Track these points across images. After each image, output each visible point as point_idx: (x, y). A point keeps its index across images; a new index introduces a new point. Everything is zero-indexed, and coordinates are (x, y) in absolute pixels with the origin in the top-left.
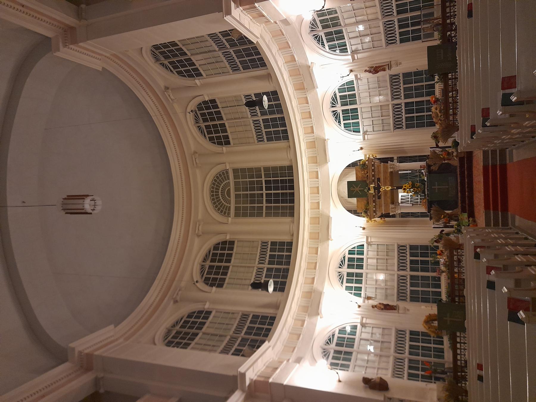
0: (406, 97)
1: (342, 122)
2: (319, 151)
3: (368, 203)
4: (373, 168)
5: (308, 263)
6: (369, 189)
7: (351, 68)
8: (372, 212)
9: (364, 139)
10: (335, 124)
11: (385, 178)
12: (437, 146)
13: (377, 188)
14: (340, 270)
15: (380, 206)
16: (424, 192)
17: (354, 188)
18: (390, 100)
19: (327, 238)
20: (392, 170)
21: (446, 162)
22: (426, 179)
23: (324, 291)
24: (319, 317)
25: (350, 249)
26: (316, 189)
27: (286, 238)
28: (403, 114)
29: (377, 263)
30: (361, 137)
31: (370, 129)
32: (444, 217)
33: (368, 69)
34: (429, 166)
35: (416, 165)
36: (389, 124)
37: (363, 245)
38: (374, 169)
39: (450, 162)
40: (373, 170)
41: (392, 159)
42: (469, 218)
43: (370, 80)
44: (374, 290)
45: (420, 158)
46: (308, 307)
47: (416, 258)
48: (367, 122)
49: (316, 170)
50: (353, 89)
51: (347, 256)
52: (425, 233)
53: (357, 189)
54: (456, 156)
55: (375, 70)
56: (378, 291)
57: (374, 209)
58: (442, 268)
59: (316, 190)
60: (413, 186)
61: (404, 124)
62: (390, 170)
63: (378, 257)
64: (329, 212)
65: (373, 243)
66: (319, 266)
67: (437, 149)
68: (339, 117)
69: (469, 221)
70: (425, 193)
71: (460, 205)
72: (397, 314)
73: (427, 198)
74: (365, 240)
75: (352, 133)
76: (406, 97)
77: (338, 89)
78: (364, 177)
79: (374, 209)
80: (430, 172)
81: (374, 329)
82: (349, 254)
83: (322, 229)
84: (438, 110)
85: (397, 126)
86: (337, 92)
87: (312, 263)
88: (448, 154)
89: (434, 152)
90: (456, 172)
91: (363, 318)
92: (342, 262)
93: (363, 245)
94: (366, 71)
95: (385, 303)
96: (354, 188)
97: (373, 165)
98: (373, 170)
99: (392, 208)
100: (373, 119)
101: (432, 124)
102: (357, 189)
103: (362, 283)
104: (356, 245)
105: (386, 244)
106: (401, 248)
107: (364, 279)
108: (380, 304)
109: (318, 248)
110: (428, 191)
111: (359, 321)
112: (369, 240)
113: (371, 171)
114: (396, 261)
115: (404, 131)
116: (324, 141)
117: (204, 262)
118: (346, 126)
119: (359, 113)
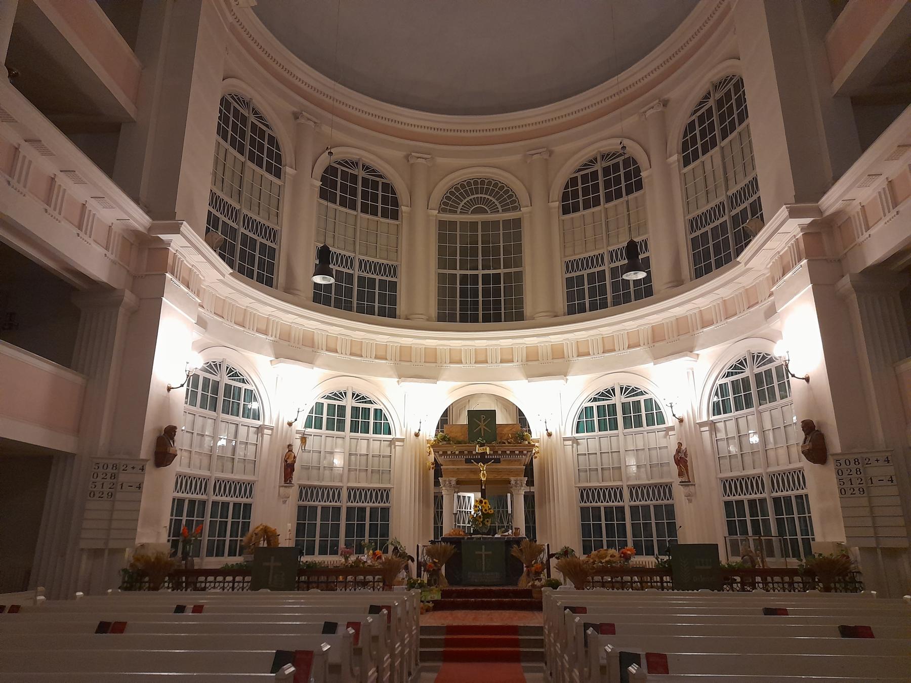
0: (634, 509)
1: (595, 405)
3: (459, 443)
4: (517, 452)
9: (565, 439)
10: (592, 392)
11: (498, 471)
12: (550, 556)
13: (483, 458)
14: (349, 395)
15: (453, 463)
16: (476, 532)
20: (513, 482)
22: (496, 536)
27: (402, 307)
28: (605, 504)
30: (568, 434)
31: (582, 449)
32: (435, 563)
33: (683, 448)
34: (518, 541)
35: (520, 521)
37: (390, 433)
39: (524, 574)
40: (512, 452)
41: (530, 483)
42: (433, 601)
43: (664, 451)
47: (365, 516)
48: (593, 445)
49: (515, 359)
50: (650, 422)
51: (372, 407)
52: (409, 531)
53: (482, 425)
54: (533, 586)
55: (681, 459)
57: (449, 452)
61: (588, 504)
62: (512, 479)
63: (370, 456)
64: (444, 380)
65: (393, 450)
69: (428, 602)
72: (278, 484)
74: (398, 436)
75: (576, 420)
76: (634, 509)
79: (449, 452)
80: (509, 543)
82: (376, 410)
83: (421, 368)
85: (585, 493)
88: (538, 573)
89: (541, 551)
93: (390, 433)
94: (680, 444)
97: (521, 453)
98: (512, 452)
100: (598, 454)
102: (482, 425)
103: (327, 429)
104: (390, 421)
106: (384, 494)
108: (295, 457)
111: (267, 423)
112: (397, 443)
118: (588, 411)
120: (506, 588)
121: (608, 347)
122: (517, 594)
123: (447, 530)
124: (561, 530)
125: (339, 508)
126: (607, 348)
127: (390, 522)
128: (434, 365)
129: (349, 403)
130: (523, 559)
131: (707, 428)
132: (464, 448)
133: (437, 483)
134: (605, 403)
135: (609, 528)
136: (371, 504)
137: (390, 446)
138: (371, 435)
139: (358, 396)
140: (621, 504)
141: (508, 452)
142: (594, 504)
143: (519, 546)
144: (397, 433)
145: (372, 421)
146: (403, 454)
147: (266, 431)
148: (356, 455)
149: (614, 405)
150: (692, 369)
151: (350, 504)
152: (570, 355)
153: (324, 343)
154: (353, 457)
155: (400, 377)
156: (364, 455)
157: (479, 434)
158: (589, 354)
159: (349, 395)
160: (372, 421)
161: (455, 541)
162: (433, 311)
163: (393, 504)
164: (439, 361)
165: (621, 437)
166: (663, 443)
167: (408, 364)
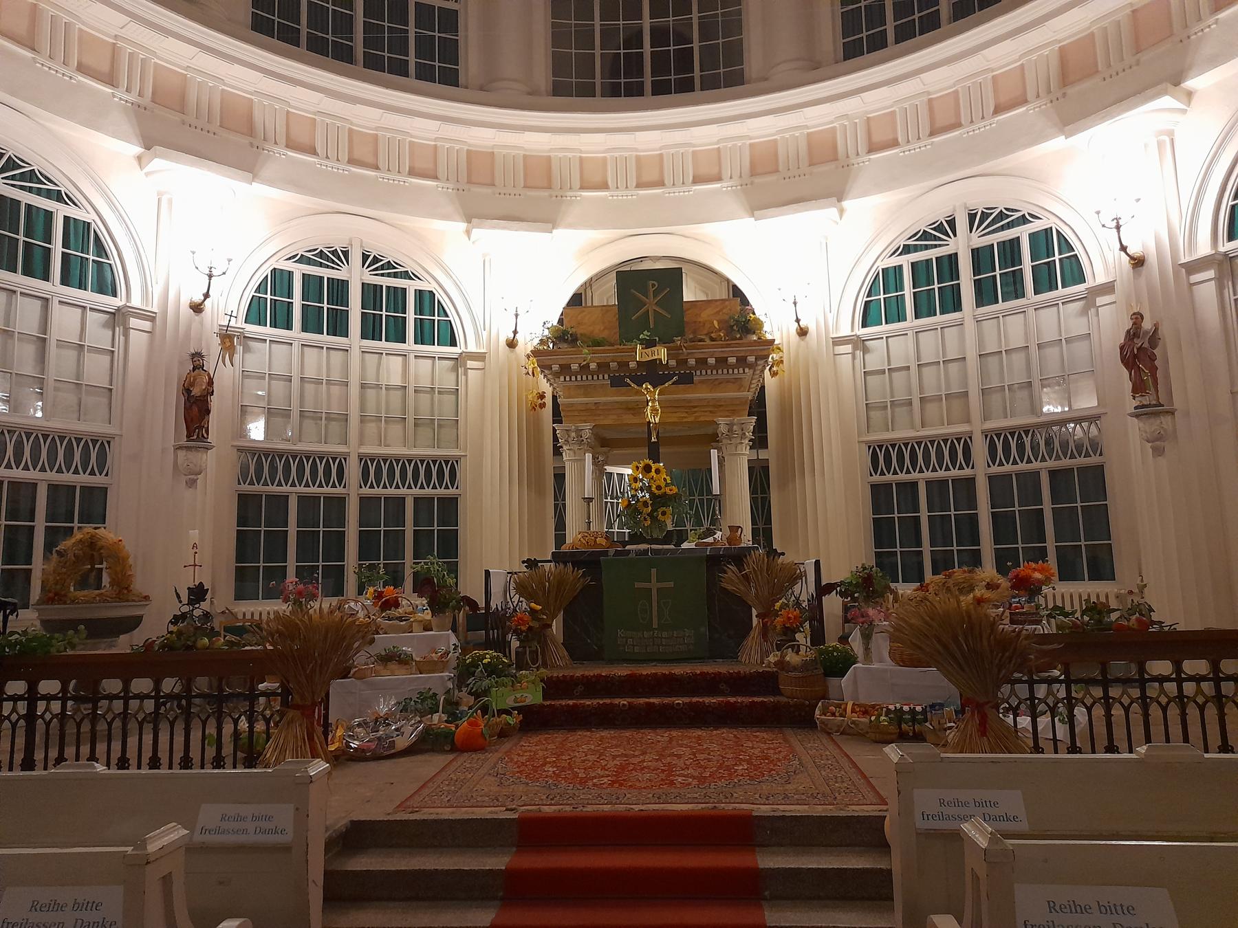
1: (906, 261)
2: (800, 178)
3: (597, 343)
4: (732, 360)
5: (376, 137)
6: (649, 344)
7: (1152, 259)
8: (563, 359)
9: (837, 342)
10: (899, 233)
11: (689, 406)
12: (823, 590)
13: (653, 373)
14: (356, 258)
15: (586, 390)
16: (635, 538)
17: (655, 294)
18: (990, 425)
19: (473, 215)
20: (723, 429)
21: (755, 621)
22: (685, 545)
23: (256, 186)
24: (138, 150)
26: (654, 176)
27: (471, 62)
29: (388, 388)
30: (845, 331)
31: (875, 360)
32: (533, 611)
33: (1147, 325)
34: (738, 557)
35: (739, 510)
36: (891, 425)
37: (453, 343)
38: (729, 366)
39: (755, 633)
40: (722, 361)
41: (760, 440)
42: (520, 710)
43: (1081, 348)
44: (955, 389)
45: (763, 529)
46: (182, 110)
47: (415, 517)
48: (902, 351)
49: (726, 173)
50: (1045, 280)
51: (411, 286)
52: (496, 547)
53: (651, 305)
54: (781, 664)
55: (1140, 353)
56: (278, 386)
57: (575, 367)
58: (772, 658)
59: (650, 174)
60: (659, 500)
61: (889, 477)
62: (722, 423)
63: (411, 391)
65: (462, 378)
66: (363, 177)
67: (812, 588)
68: (927, 247)
69: (508, 712)
70: (631, 542)
71: (578, 673)
72: (171, 442)
73: (612, 551)
74: (472, 348)
77: (1048, 232)
78: (694, 332)
79: (575, 367)
80: (715, 561)
81: (107, 358)
82: (420, 294)
83: (516, 196)
84: (988, 594)
85: (882, 455)
86: (1036, 226)
87: (376, 154)
88: (789, 633)
89: (794, 576)
90: (713, 656)
91: (151, 318)
92: (389, 265)
93: (453, 343)
94: (1138, 318)
95: (215, 402)
96: (655, 294)
97: (742, 361)
98: (722, 361)
99: (578, 431)
100: (914, 368)
101: (245, 585)
102: (651, 305)
103: (305, 329)
104: (453, 317)
105: (461, 418)
106: (447, 470)
107: (325, 338)
108: (211, 382)
109: (435, 178)
110: (639, 553)
111: (136, 301)
112: (470, 364)
113: (719, 352)
114: (397, 450)
115: (862, 479)
116: (836, 194)
117: (365, 257)
118: (891, 277)
119: (939, 318)
121: (942, 119)
122: (740, 684)
123: (573, 533)
125: (971, 481)
126: (940, 123)
127: (460, 528)
128: (545, 193)
129: (356, 275)
131: (1211, 274)
132: (605, 355)
133: (557, 451)
134: (932, 254)
135: (939, 524)
136: (416, 491)
137: (455, 369)
138: (410, 345)
139: (376, 260)
140: (967, 472)
141: (712, 361)
143: (741, 569)
144: (469, 342)
145: (411, 316)
146: (484, 387)
147: (134, 322)
148: (378, 387)
149: (953, 258)
150: (1171, 134)
151: (366, 491)
152: (851, 152)
153: (281, 130)
154: (371, 393)
155: (468, 219)
157: (644, 324)
158: (894, 143)
159: (356, 258)
160: (411, 316)
161: (587, 561)
162: (542, 75)
163: (466, 489)
164: (556, 182)
165: (970, 325)
166: (1078, 326)
167: (488, 190)
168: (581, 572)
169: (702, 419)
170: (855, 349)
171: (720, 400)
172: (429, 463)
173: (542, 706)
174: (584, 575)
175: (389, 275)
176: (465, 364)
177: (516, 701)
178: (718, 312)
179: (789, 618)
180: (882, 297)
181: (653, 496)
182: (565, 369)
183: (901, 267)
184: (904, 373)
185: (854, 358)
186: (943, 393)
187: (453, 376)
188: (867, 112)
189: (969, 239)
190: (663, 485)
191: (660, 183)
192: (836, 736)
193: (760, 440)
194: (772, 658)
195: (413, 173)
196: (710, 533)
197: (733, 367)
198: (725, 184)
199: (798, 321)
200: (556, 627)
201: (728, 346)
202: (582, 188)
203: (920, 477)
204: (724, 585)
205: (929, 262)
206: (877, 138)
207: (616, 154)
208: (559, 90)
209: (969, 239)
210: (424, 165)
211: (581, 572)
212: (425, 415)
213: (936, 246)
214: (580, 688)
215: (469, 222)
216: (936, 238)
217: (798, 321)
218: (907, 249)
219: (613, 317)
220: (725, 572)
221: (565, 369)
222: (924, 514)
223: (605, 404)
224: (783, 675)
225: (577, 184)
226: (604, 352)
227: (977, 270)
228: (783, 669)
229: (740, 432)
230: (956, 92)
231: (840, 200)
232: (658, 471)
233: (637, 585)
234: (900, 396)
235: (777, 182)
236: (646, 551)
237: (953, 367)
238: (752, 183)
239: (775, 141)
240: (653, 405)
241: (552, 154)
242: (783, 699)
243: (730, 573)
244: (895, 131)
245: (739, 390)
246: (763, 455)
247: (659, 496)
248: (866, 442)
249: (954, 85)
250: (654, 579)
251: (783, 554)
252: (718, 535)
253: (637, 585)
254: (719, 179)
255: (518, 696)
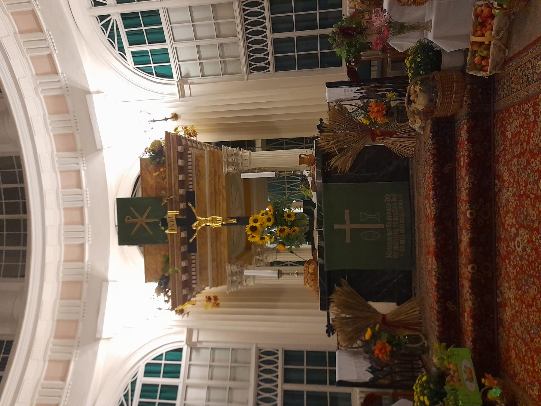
1: (129, 50)
9: (182, 94)
10: (110, 54)
11: (215, 193)
15: (204, 268)
17: (134, 217)
19: (94, 338)
20: (231, 169)
22: (315, 200)
25: (149, 359)
28: (268, 31)
30: (174, 89)
31: (194, 69)
34: (324, 157)
35: (288, 158)
37: (180, 350)
40: (182, 170)
42: (480, 376)
49: (74, 167)
53: (142, 220)
54: (426, 114)
58: (417, 124)
59: (75, 216)
61: (271, 59)
62: (225, 170)
64: (107, 268)
65: (204, 345)
68: (119, 35)
73: (319, 260)
74: (183, 337)
75: (154, 78)
80: (327, 175)
82: (147, 373)
85: (256, 64)
93: (180, 350)
96: (134, 217)
98: (182, 170)
100: (198, 43)
102: (142, 220)
104: (163, 351)
106: (265, 357)
109: (68, 362)
112: (194, 339)
113: (174, 172)
116: (85, 93)
118: (140, 59)
119: (164, 26)
120: (464, 195)
122: (444, 153)
124: (308, 97)
128: (85, 286)
129: (115, 11)
130: (359, 146)
134: (123, 32)
136: (280, 381)
141: (181, 177)
142: (270, 50)
144: (179, 340)
149: (125, 17)
152: (57, 86)
156: (208, 394)
158: (50, 56)
163: (279, 344)
168: (337, 288)
169: (224, 184)
170: (186, 83)
171: (210, 171)
172: (260, 371)
173: (474, 351)
174: (340, 285)
175: (132, 396)
176: (194, 342)
177: (471, 380)
178: (150, 172)
179: (378, 111)
180: (152, 65)
181: (275, 225)
182: (187, 284)
183: (133, 53)
184: (202, 50)
185: (193, 83)
186: (213, 22)
187: (203, 351)
188: (32, 75)
189: (111, 5)
190: (266, 217)
191: (81, 209)
192: (516, 47)
193: (249, 145)
194: (417, 124)
195: (64, 379)
196: (304, 179)
197: (186, 161)
198: (82, 168)
199: (166, 119)
200: (383, 308)
201: (170, 165)
202: (82, 260)
203: (270, 36)
204: (347, 169)
205: (128, 34)
206: (48, 69)
207: (62, 238)
208: (23, 276)
209: (111, 5)
210: (60, 369)
211: (337, 288)
212: (227, 373)
213: (118, 29)
214: (449, 305)
215: (99, 339)
216: (112, 29)
217: (166, 119)
218: (121, 49)
219: (151, 248)
220: (336, 168)
221: (187, 284)
222: (295, 34)
223: (213, 254)
224: (438, 113)
225: (79, 264)
226: (173, 256)
227: (145, 14)
228: (433, 112)
229: (233, 157)
230: (12, 14)
231: (89, 93)
232: (256, 221)
233: (348, 240)
234: (216, 52)
235: (78, 134)
236: (320, 233)
237: (196, 15)
238: (81, 150)
239: (54, 135)
240: (210, 222)
241: (61, 280)
242: (465, 110)
243: (338, 163)
244: (42, 57)
245: (203, 158)
246: (259, 143)
247: (275, 220)
248: (248, 75)
249: (7, 15)
250: (342, 227)
251: (321, 120)
252: (306, 173)
253: (348, 240)
254: (78, 172)
255: (465, 376)
